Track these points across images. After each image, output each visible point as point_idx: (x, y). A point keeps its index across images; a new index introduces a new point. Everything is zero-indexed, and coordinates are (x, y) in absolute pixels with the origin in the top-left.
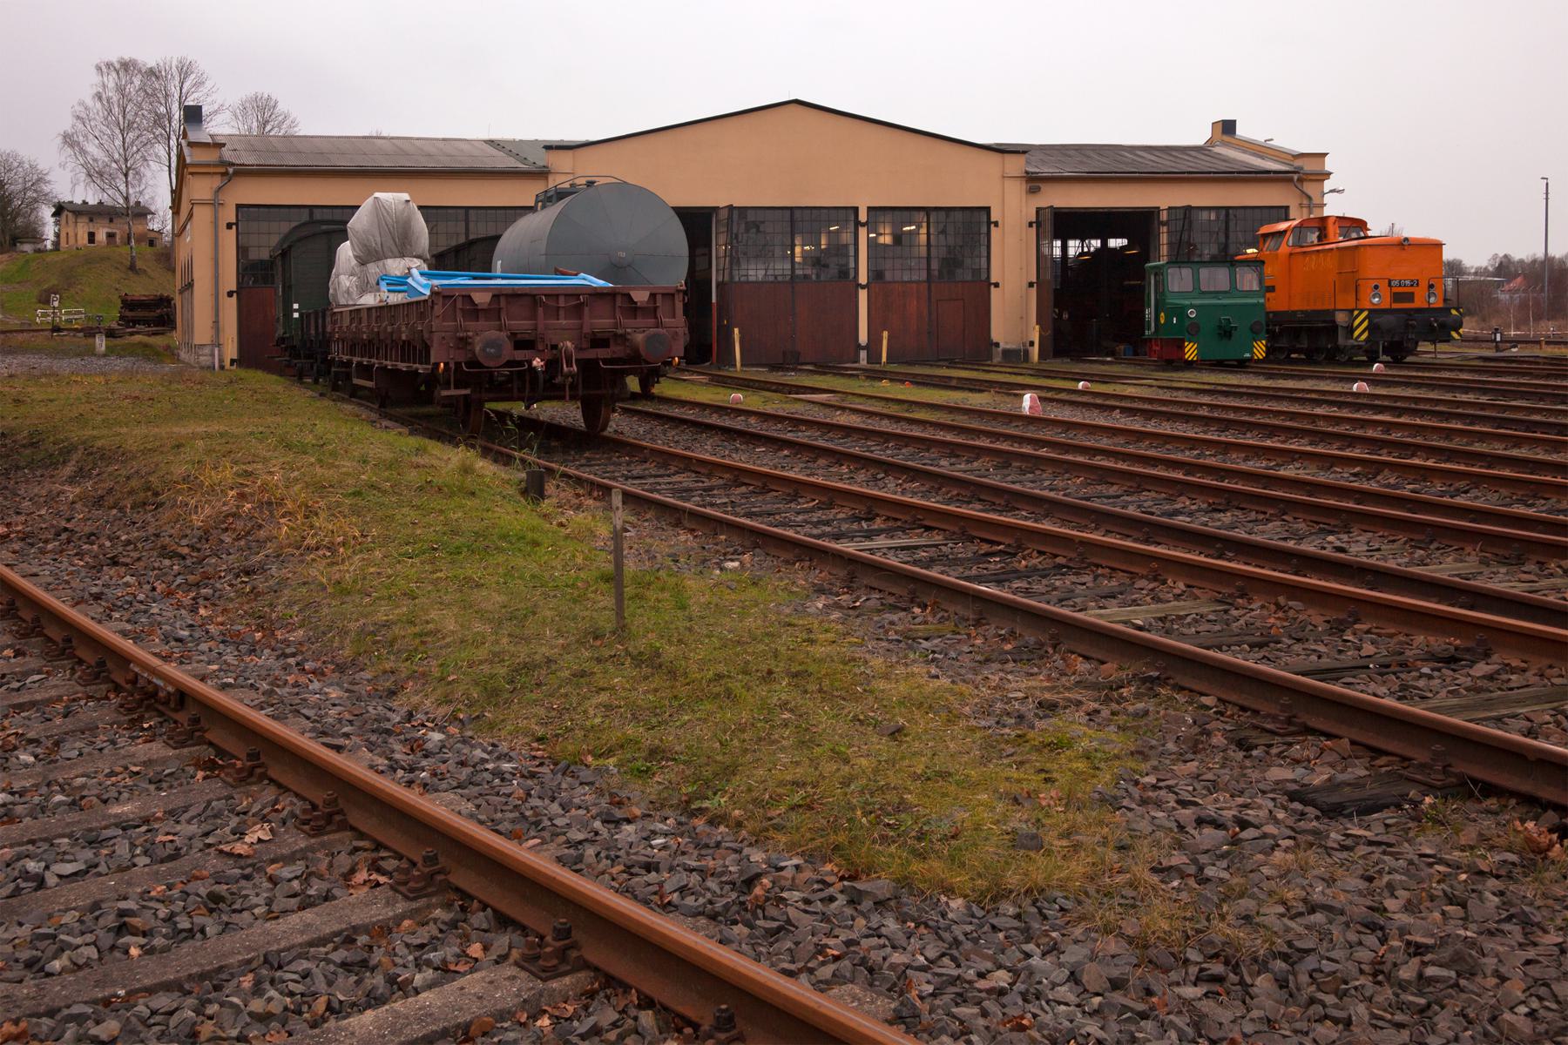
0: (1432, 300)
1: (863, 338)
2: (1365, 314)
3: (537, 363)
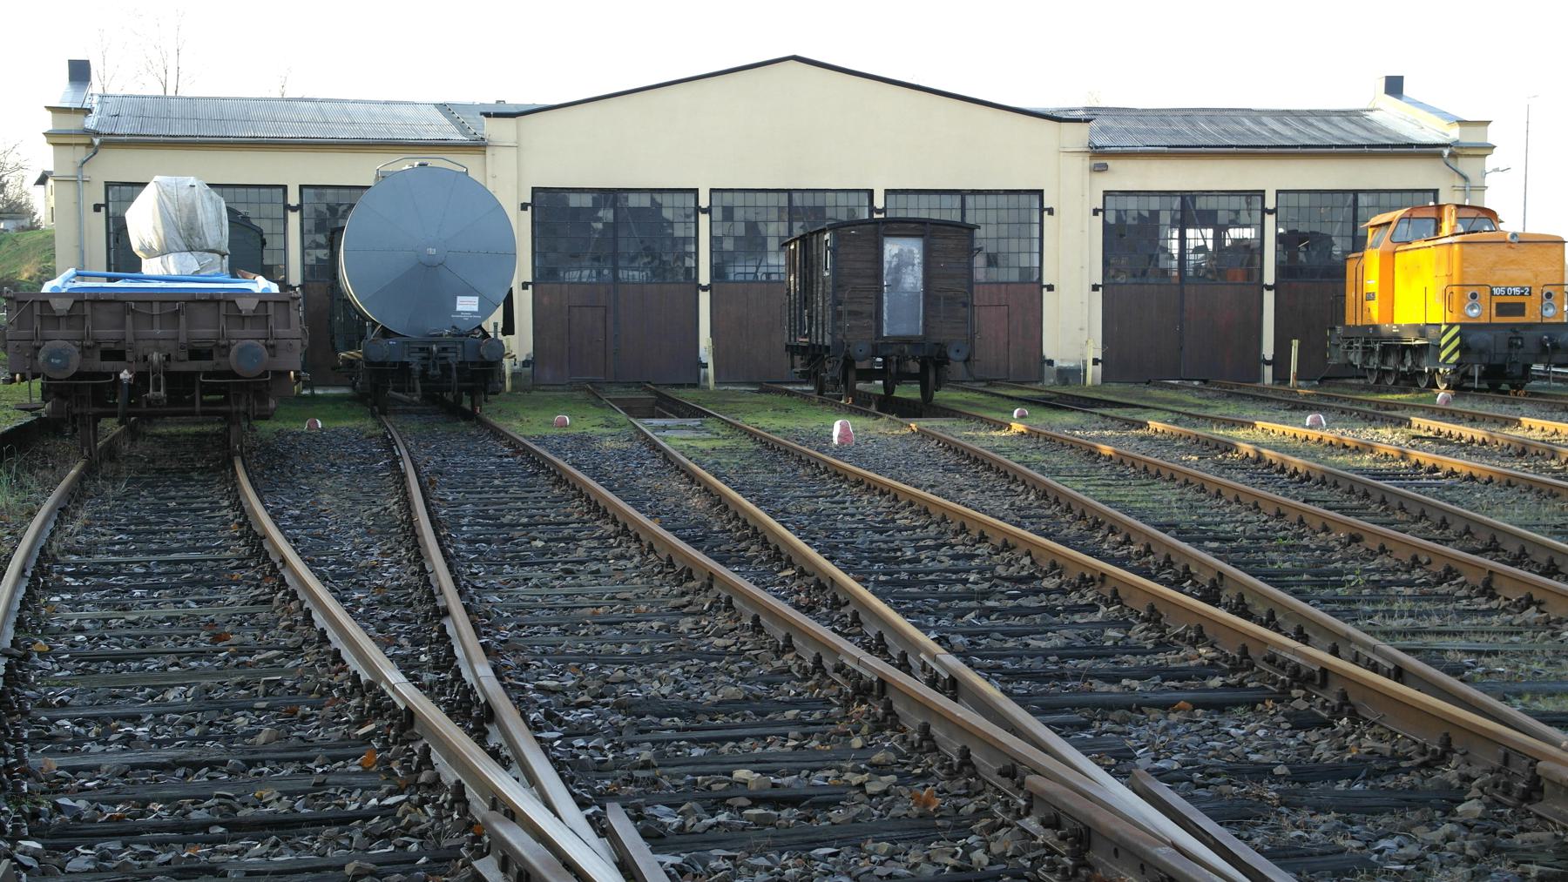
1: (1268, 351)
2: (1456, 329)
3: (125, 375)
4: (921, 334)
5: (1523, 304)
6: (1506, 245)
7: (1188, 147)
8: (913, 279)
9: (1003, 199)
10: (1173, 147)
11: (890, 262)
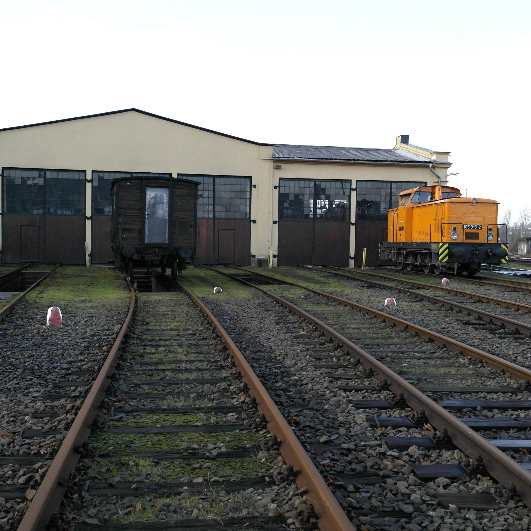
0: (491, 237)
1: (352, 253)
2: (447, 245)
4: (167, 242)
5: (478, 234)
6: (469, 204)
7: (317, 159)
8: (163, 211)
9: (233, 180)
10: (311, 158)
11: (150, 202)
